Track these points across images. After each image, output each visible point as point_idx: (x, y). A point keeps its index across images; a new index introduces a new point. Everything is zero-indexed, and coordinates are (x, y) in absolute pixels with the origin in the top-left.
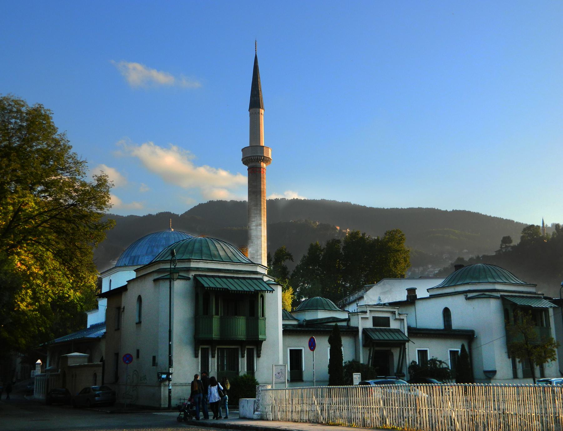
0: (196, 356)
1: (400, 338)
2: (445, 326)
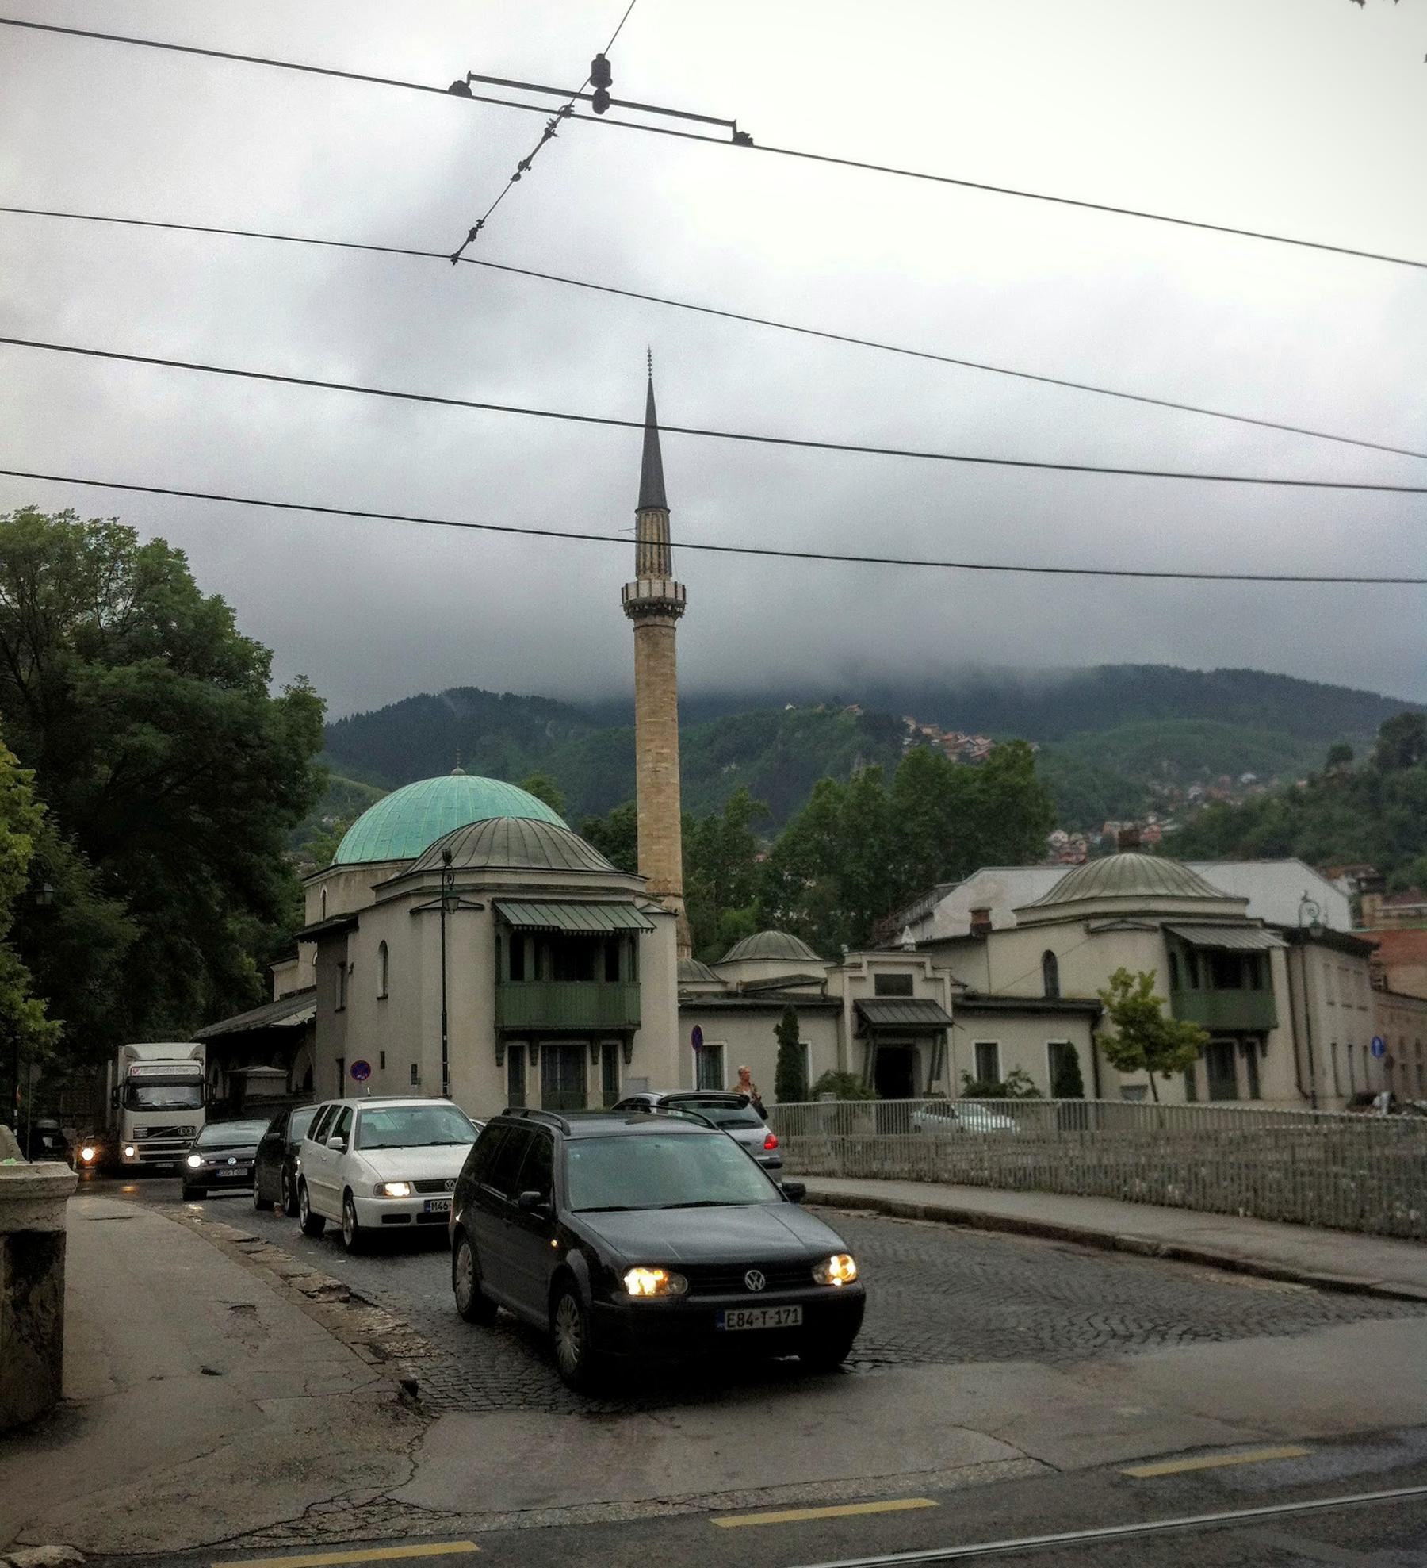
0: (500, 1064)
1: (934, 1019)
2: (1047, 991)
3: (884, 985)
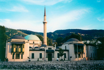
0: (12, 54)
3: (49, 48)
